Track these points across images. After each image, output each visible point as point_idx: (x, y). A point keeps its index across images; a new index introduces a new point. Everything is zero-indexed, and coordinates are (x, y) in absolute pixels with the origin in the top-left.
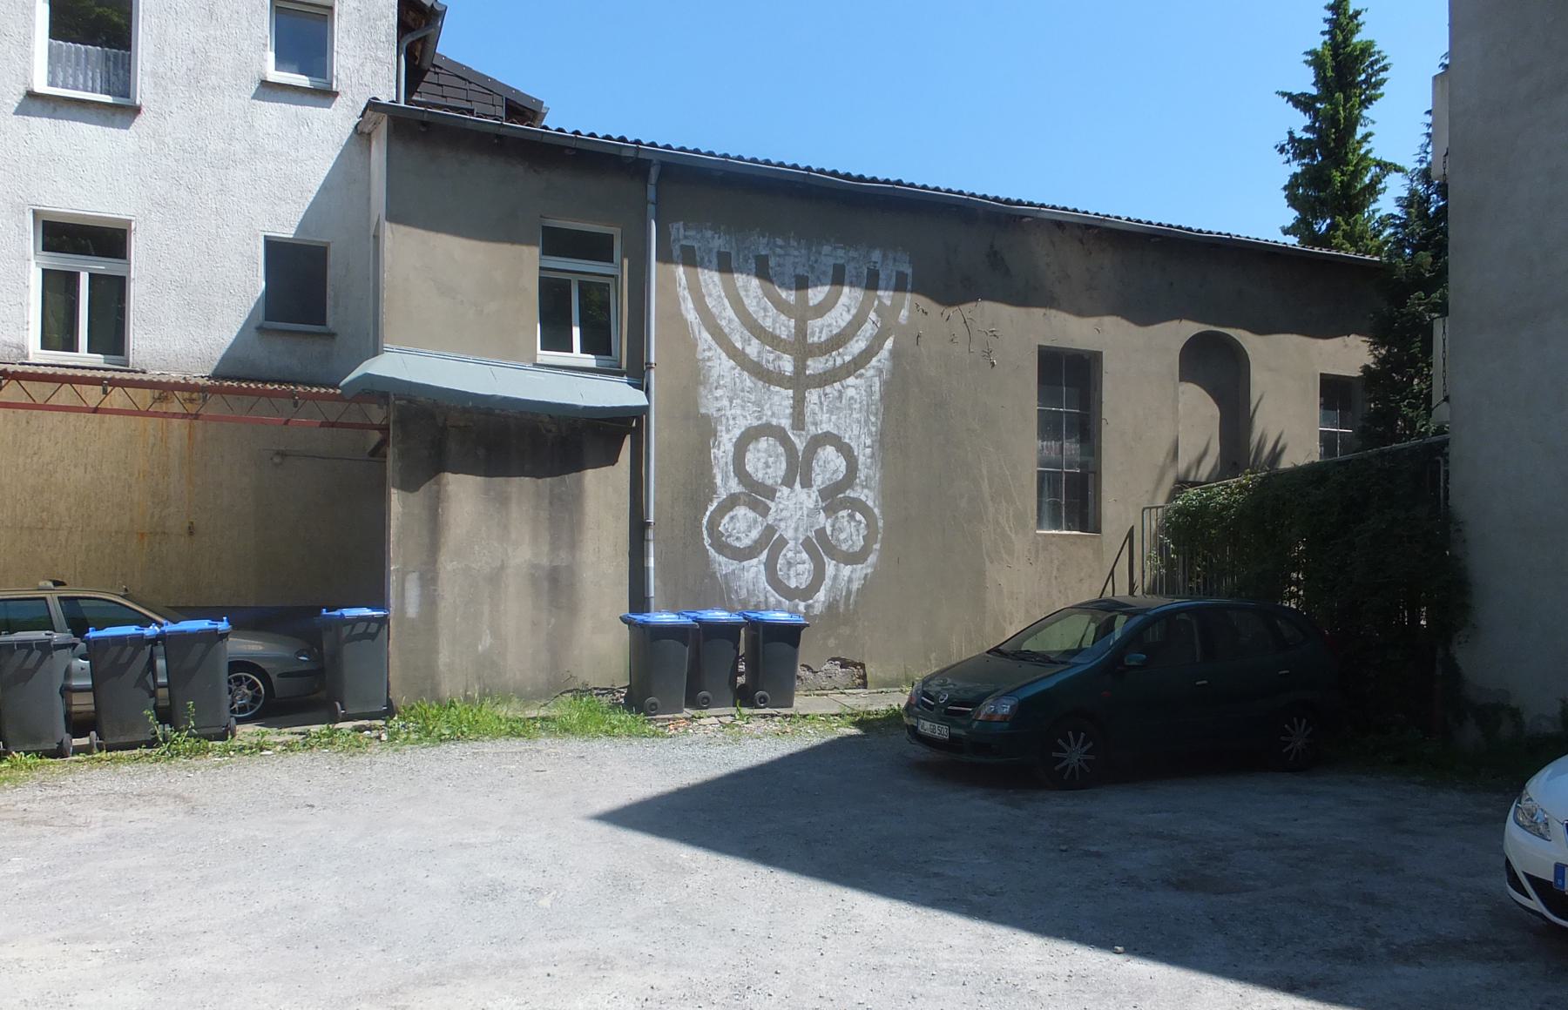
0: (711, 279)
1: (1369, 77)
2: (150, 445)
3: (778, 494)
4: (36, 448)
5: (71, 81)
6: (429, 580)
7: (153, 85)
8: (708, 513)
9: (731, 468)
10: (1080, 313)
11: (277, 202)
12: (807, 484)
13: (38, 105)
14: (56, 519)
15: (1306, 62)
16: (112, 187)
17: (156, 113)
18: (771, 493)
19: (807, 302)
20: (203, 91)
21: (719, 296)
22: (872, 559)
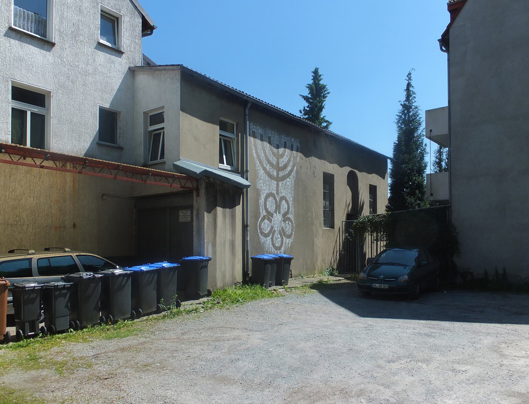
0: (258, 142)
1: (324, 95)
2: (59, 189)
3: (274, 216)
4: (13, 189)
5: (22, 25)
6: (214, 245)
7: (59, 35)
8: (259, 222)
9: (264, 206)
10: (330, 163)
11: (103, 93)
12: (280, 213)
13: (14, 34)
14: (22, 221)
15: (306, 87)
16: (44, 76)
17: (60, 47)
18: (272, 215)
19: (279, 153)
20: (77, 42)
21: (261, 149)
22: (293, 236)
